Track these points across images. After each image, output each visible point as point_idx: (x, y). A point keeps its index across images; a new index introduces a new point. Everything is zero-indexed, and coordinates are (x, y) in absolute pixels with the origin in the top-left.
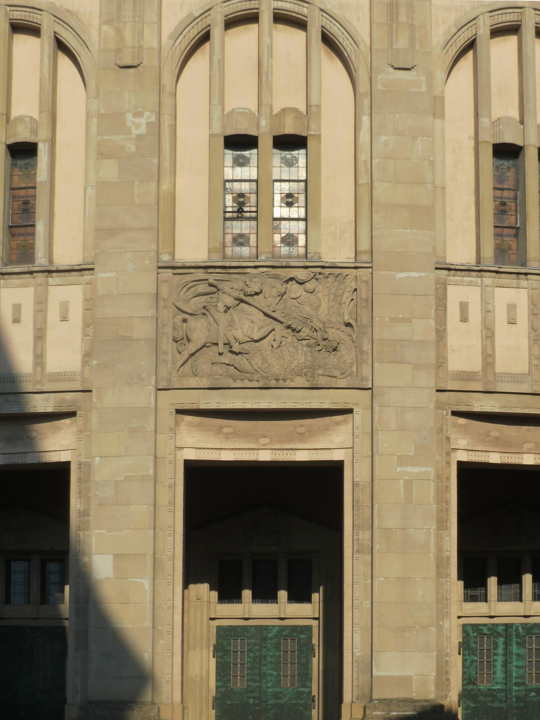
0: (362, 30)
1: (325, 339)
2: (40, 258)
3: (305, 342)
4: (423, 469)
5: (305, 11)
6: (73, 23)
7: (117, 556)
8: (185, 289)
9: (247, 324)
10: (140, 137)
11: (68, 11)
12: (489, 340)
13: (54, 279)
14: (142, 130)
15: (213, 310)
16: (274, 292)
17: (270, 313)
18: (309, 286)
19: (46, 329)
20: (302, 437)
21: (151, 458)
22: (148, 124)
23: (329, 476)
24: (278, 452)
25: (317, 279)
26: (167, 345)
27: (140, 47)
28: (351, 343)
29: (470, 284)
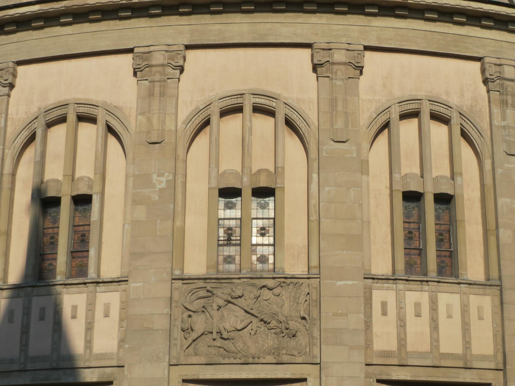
0: (312, 115)
1: (287, 329)
2: (92, 274)
3: (273, 331)
5: (274, 104)
6: (119, 115)
8: (190, 294)
9: (233, 318)
11: (115, 106)
13: (101, 288)
14: (163, 185)
15: (209, 309)
16: (252, 296)
19: (94, 322)
22: (167, 181)
25: (281, 286)
26: (177, 333)
27: (163, 130)
28: (305, 331)
29: (388, 289)
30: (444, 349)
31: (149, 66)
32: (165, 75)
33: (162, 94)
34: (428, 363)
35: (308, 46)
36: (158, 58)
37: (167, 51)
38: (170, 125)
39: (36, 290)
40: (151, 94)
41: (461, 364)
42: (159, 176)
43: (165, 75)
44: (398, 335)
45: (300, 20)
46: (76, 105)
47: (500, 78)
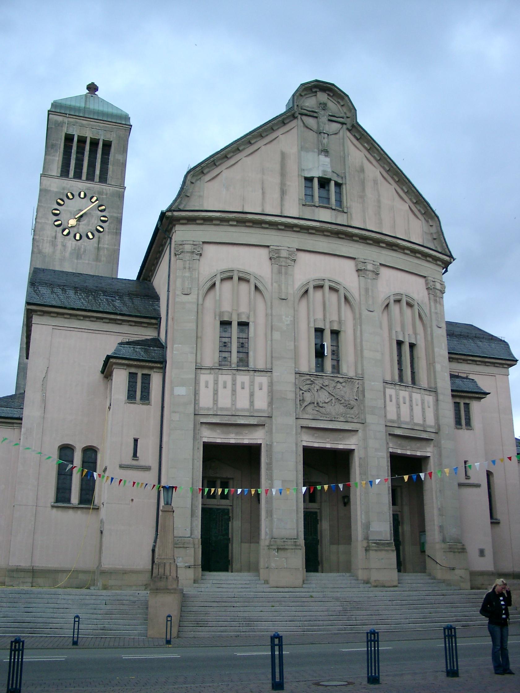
0: (356, 294)
2: (251, 365)
5: (338, 287)
9: (323, 396)
10: (288, 325)
13: (257, 374)
15: (312, 390)
16: (332, 386)
18: (343, 384)
20: (341, 439)
21: (294, 444)
29: (392, 388)
30: (416, 421)
31: (279, 257)
32: (287, 263)
33: (286, 273)
36: (284, 254)
38: (291, 291)
40: (280, 272)
44: (397, 412)
47: (434, 288)
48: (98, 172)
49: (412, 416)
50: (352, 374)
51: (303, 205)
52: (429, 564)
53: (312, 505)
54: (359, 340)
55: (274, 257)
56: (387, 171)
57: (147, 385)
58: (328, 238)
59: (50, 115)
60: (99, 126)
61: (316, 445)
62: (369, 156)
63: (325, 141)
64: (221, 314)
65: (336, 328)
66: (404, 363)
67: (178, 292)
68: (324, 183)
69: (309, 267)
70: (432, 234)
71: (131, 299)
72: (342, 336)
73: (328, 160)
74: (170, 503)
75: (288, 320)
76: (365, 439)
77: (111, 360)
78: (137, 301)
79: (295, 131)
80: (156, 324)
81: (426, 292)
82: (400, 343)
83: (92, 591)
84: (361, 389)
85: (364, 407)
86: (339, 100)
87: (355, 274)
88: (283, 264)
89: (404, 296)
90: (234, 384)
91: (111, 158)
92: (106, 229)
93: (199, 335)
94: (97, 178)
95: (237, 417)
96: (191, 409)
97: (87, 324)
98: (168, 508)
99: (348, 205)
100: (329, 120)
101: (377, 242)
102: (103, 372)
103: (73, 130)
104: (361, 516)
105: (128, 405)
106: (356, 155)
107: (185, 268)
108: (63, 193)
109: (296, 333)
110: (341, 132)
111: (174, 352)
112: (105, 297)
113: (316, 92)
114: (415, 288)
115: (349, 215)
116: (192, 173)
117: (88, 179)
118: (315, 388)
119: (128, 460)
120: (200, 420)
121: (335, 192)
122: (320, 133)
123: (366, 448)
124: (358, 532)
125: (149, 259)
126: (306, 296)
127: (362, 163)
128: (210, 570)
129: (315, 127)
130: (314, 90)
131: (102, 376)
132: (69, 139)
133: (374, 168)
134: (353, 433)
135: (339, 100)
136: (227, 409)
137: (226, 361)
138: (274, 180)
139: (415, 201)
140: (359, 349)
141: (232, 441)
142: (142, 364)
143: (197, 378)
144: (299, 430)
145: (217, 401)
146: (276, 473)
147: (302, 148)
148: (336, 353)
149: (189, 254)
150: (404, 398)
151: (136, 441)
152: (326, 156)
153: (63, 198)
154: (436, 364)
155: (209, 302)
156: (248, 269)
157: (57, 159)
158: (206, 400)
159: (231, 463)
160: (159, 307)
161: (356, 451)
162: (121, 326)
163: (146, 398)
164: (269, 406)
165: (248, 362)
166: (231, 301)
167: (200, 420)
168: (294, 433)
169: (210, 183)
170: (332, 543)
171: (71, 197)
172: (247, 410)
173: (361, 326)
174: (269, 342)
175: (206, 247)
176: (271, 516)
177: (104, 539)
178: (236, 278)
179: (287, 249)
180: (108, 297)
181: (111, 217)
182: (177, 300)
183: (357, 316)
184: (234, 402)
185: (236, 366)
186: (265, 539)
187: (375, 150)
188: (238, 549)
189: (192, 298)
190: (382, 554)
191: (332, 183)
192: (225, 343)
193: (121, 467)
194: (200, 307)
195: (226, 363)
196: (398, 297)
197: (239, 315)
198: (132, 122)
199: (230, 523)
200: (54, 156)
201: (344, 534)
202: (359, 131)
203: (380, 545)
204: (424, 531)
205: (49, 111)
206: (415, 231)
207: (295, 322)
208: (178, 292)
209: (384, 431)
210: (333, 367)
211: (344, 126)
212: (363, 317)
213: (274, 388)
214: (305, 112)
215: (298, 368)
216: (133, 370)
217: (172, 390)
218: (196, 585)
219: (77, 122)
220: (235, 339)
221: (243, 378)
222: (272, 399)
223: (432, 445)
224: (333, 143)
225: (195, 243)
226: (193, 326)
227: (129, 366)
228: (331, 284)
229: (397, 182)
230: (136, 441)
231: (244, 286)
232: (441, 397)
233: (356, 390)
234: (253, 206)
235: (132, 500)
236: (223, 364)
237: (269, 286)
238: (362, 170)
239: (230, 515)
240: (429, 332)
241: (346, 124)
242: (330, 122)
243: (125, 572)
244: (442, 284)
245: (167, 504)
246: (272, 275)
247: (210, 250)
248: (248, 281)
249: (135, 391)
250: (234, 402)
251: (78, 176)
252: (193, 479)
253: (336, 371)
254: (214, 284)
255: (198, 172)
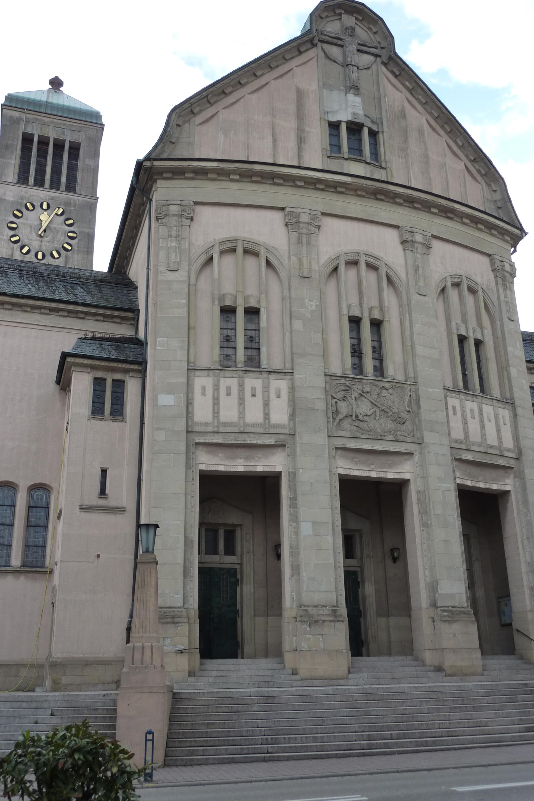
0: (402, 274)
2: (264, 364)
3: (390, 418)
4: (449, 485)
5: (378, 264)
6: (276, 253)
7: (314, 523)
9: (364, 408)
11: (273, 247)
12: (466, 425)
13: (272, 376)
14: (313, 308)
15: (349, 399)
16: (375, 392)
17: (374, 402)
18: (391, 391)
19: (269, 401)
22: (316, 305)
23: (398, 488)
24: (379, 473)
27: (310, 269)
29: (455, 398)
30: (489, 442)
32: (309, 230)
33: (308, 244)
34: (481, 449)
35: (397, 227)
36: (304, 218)
37: (310, 214)
38: (315, 267)
39: (222, 373)
40: (300, 242)
41: (498, 452)
42: (309, 301)
43: (309, 230)
44: (464, 429)
45: (392, 209)
46: (243, 242)
48: (64, 179)
49: (483, 435)
50: (400, 377)
51: (328, 157)
52: (519, 640)
53: (352, 562)
54: (408, 333)
55: (292, 222)
56: (436, 119)
57: (119, 395)
58: (363, 199)
59: (4, 110)
60: (64, 124)
61: (356, 473)
62: (411, 98)
63: (355, 76)
64: (221, 298)
65: (377, 315)
66: (468, 367)
67: (162, 268)
68: (355, 128)
69: (338, 238)
70: (495, 201)
71: (99, 287)
72: (386, 329)
73: (358, 100)
74: (151, 549)
75: (313, 305)
76: (423, 465)
77: (69, 359)
78: (106, 290)
79: (314, 62)
80: (133, 319)
81: (492, 275)
82: (462, 339)
83: (39, 693)
84: (414, 397)
85: (420, 421)
86: (371, 26)
87: (400, 248)
88: (304, 231)
89: (464, 278)
90: (241, 389)
91: (80, 163)
92: (75, 247)
93: (192, 325)
94: (63, 186)
95: (246, 435)
96: (181, 425)
97: (36, 318)
98: (148, 556)
99: (387, 158)
100: (359, 51)
101: (426, 207)
102: (58, 382)
103: (33, 129)
104: (424, 573)
105: (93, 421)
106: (395, 96)
107: (170, 236)
108: (21, 204)
109: (324, 322)
110: (374, 67)
111: (157, 348)
112: (62, 283)
113: (340, 14)
114: (477, 268)
115: (389, 172)
116: (177, 111)
117: (51, 187)
118: (353, 396)
119: (94, 499)
120: (194, 439)
121: (370, 143)
122: (347, 65)
123: (425, 478)
124: (421, 597)
125: (123, 239)
126: (335, 274)
127: (403, 106)
128: (211, 658)
129: (340, 59)
130: (338, 11)
131: (58, 387)
132: (27, 139)
133: (419, 115)
134: (407, 457)
135: (371, 26)
136: (232, 424)
137: (229, 360)
138: (288, 125)
139: (472, 158)
140: (409, 344)
141: (241, 469)
142: (113, 365)
143: (190, 382)
144: (333, 452)
145: (218, 413)
146: (303, 511)
147: (325, 85)
148: (378, 352)
149: (176, 218)
150: (472, 411)
151: (104, 472)
152: (356, 95)
153: (21, 209)
154: (511, 368)
155: (204, 283)
156: (256, 238)
157: (13, 162)
158: (202, 413)
159: (239, 503)
160: (137, 297)
161: (411, 481)
162: (85, 321)
163: (118, 412)
164: (290, 420)
165: (259, 362)
166: (233, 280)
167: (194, 439)
168: (327, 455)
169: (203, 128)
170: (379, 615)
171: (31, 208)
172: (261, 426)
173: (410, 315)
174: (288, 334)
175: (198, 208)
176: (299, 574)
177: (55, 615)
178: (240, 250)
179: (309, 211)
180: (66, 284)
181: (81, 233)
182: (160, 278)
183: (405, 302)
184: (242, 414)
185: (243, 365)
186: (291, 608)
187: (419, 90)
188: (251, 626)
189: (181, 275)
190: (456, 627)
191: (365, 131)
192: (228, 336)
193: (82, 508)
194: (192, 288)
195: (230, 363)
196: (457, 280)
197: (245, 299)
198: (104, 121)
199: (238, 589)
200: (9, 158)
201: (399, 600)
202: (397, 64)
203: (452, 614)
204: (509, 596)
205: (2, 105)
206: (475, 195)
207: (322, 307)
208: (162, 268)
209: (449, 454)
210: (375, 368)
211: (378, 59)
212: (413, 302)
213: (298, 395)
214: (327, 38)
215: (328, 369)
216: (100, 374)
217: (155, 400)
218: (192, 679)
219: (37, 119)
220: (240, 331)
221: (253, 382)
222: (294, 410)
223: (512, 476)
224: (365, 80)
225: (184, 203)
226: (184, 312)
227: (93, 368)
228: (368, 259)
229: (448, 133)
230: (104, 472)
231: (251, 262)
232: (519, 411)
233: (407, 398)
234: (262, 152)
235: (98, 556)
236: (226, 362)
237: (286, 262)
238: (403, 115)
239: (239, 577)
240: (499, 326)
241: (380, 56)
242: (360, 54)
243: (87, 663)
244: (512, 265)
245: (147, 551)
246: (289, 247)
247: (205, 214)
248: (256, 254)
249: (103, 403)
250: (242, 414)
251: (39, 183)
252: (185, 522)
253: (378, 374)
254: (211, 259)
255: (185, 114)
